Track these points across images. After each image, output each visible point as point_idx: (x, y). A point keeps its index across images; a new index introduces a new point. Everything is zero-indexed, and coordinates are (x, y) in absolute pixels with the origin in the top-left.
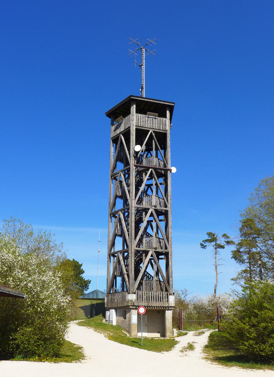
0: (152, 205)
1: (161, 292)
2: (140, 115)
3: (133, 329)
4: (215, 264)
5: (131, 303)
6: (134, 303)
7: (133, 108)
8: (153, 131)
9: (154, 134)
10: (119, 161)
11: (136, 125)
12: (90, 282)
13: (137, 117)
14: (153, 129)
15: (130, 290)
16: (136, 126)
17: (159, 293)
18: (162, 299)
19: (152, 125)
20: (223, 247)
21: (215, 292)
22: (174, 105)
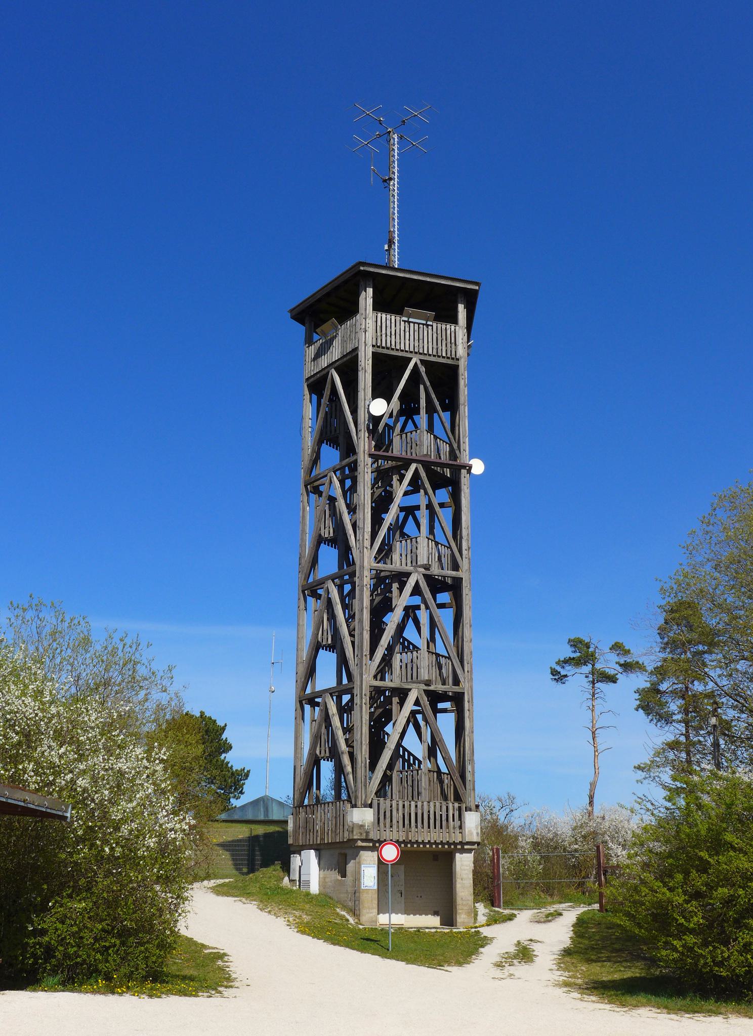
1: (444, 803)
4: (590, 726)
5: (361, 834)
6: (367, 833)
7: (367, 298)
9: (422, 369)
11: (374, 344)
14: (420, 354)
16: (373, 346)
17: (438, 805)
18: (444, 823)
19: (416, 344)
22: (477, 288)
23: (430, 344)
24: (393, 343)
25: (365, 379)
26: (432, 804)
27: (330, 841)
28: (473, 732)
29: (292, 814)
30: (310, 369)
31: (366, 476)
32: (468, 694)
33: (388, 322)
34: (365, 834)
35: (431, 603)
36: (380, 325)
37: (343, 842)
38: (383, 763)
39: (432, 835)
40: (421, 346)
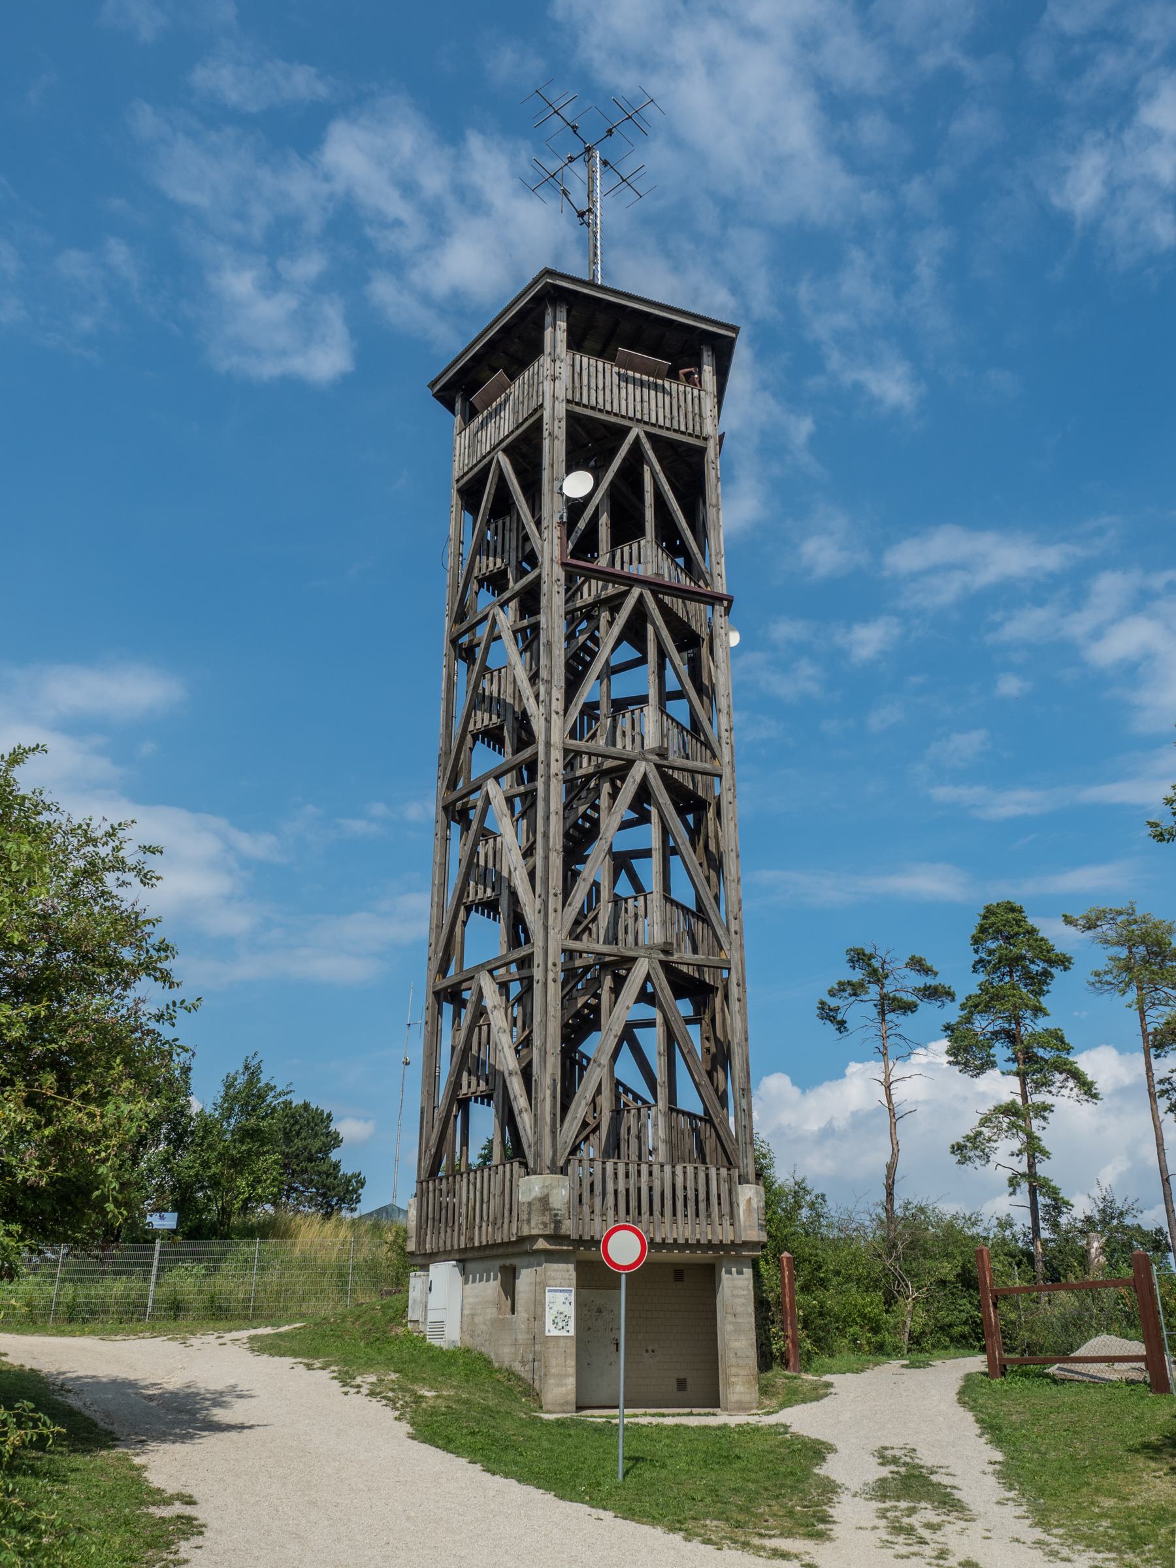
0: (646, 748)
1: (701, 1168)
2: (585, 360)
3: (553, 1371)
4: (882, 1077)
5: (545, 1225)
6: (558, 1224)
7: (556, 334)
8: (646, 432)
9: (647, 446)
10: (483, 742)
11: (570, 397)
12: (362, 1184)
13: (573, 366)
14: (646, 423)
15: (537, 1155)
16: (568, 401)
17: (690, 1169)
18: (702, 1206)
19: (638, 408)
20: (909, 1008)
21: (890, 1194)
22: (734, 335)
23: (661, 411)
24: (601, 401)
25: (554, 448)
26: (679, 1169)
27: (484, 1243)
28: (746, 1040)
29: (415, 1196)
30: (461, 463)
31: (554, 602)
32: (737, 972)
33: (593, 370)
34: (552, 1226)
35: (670, 813)
36: (579, 370)
37: (510, 1243)
38: (585, 1090)
39: (681, 1229)
40: (646, 411)
